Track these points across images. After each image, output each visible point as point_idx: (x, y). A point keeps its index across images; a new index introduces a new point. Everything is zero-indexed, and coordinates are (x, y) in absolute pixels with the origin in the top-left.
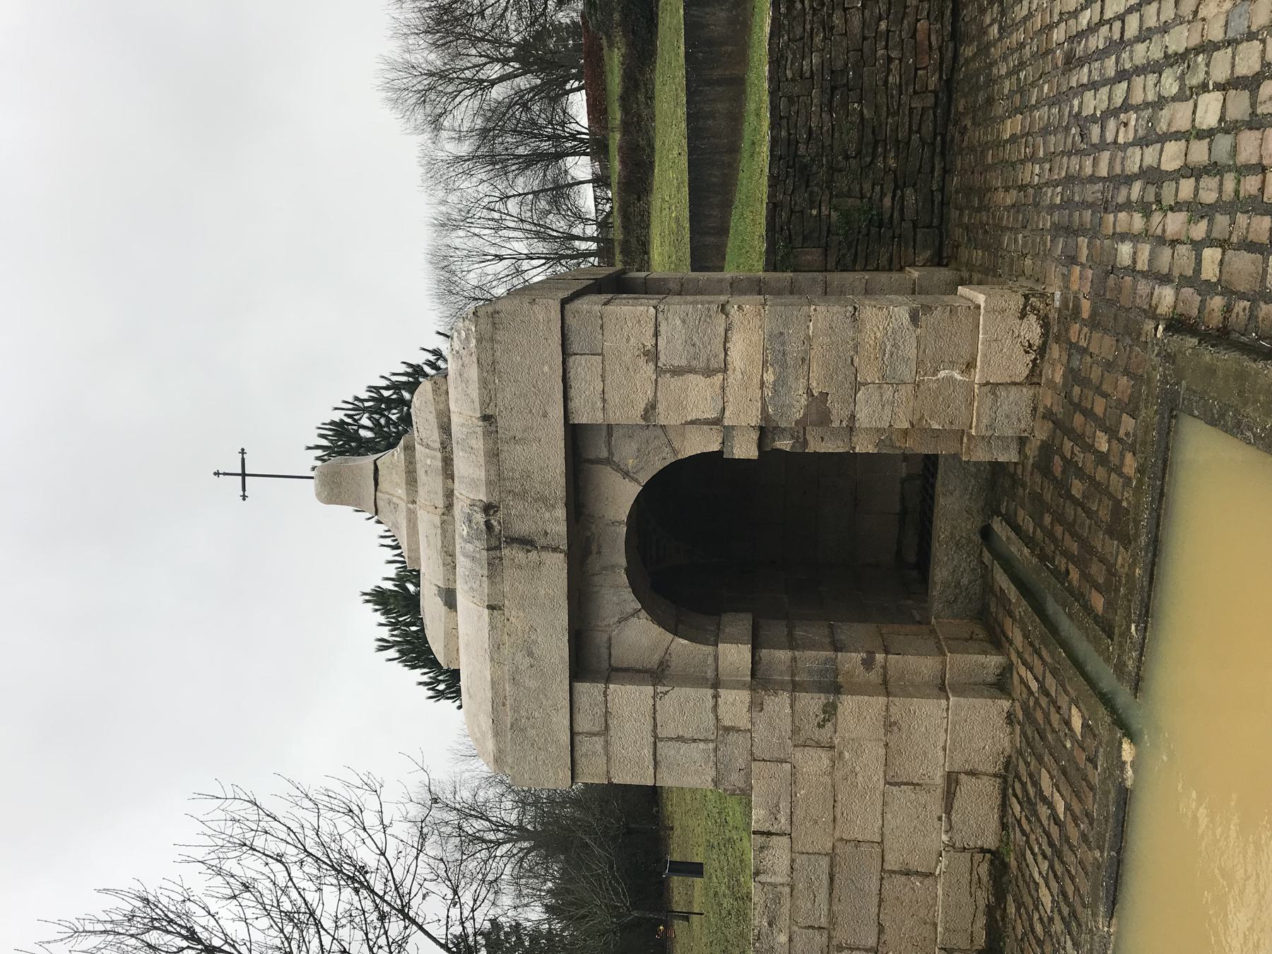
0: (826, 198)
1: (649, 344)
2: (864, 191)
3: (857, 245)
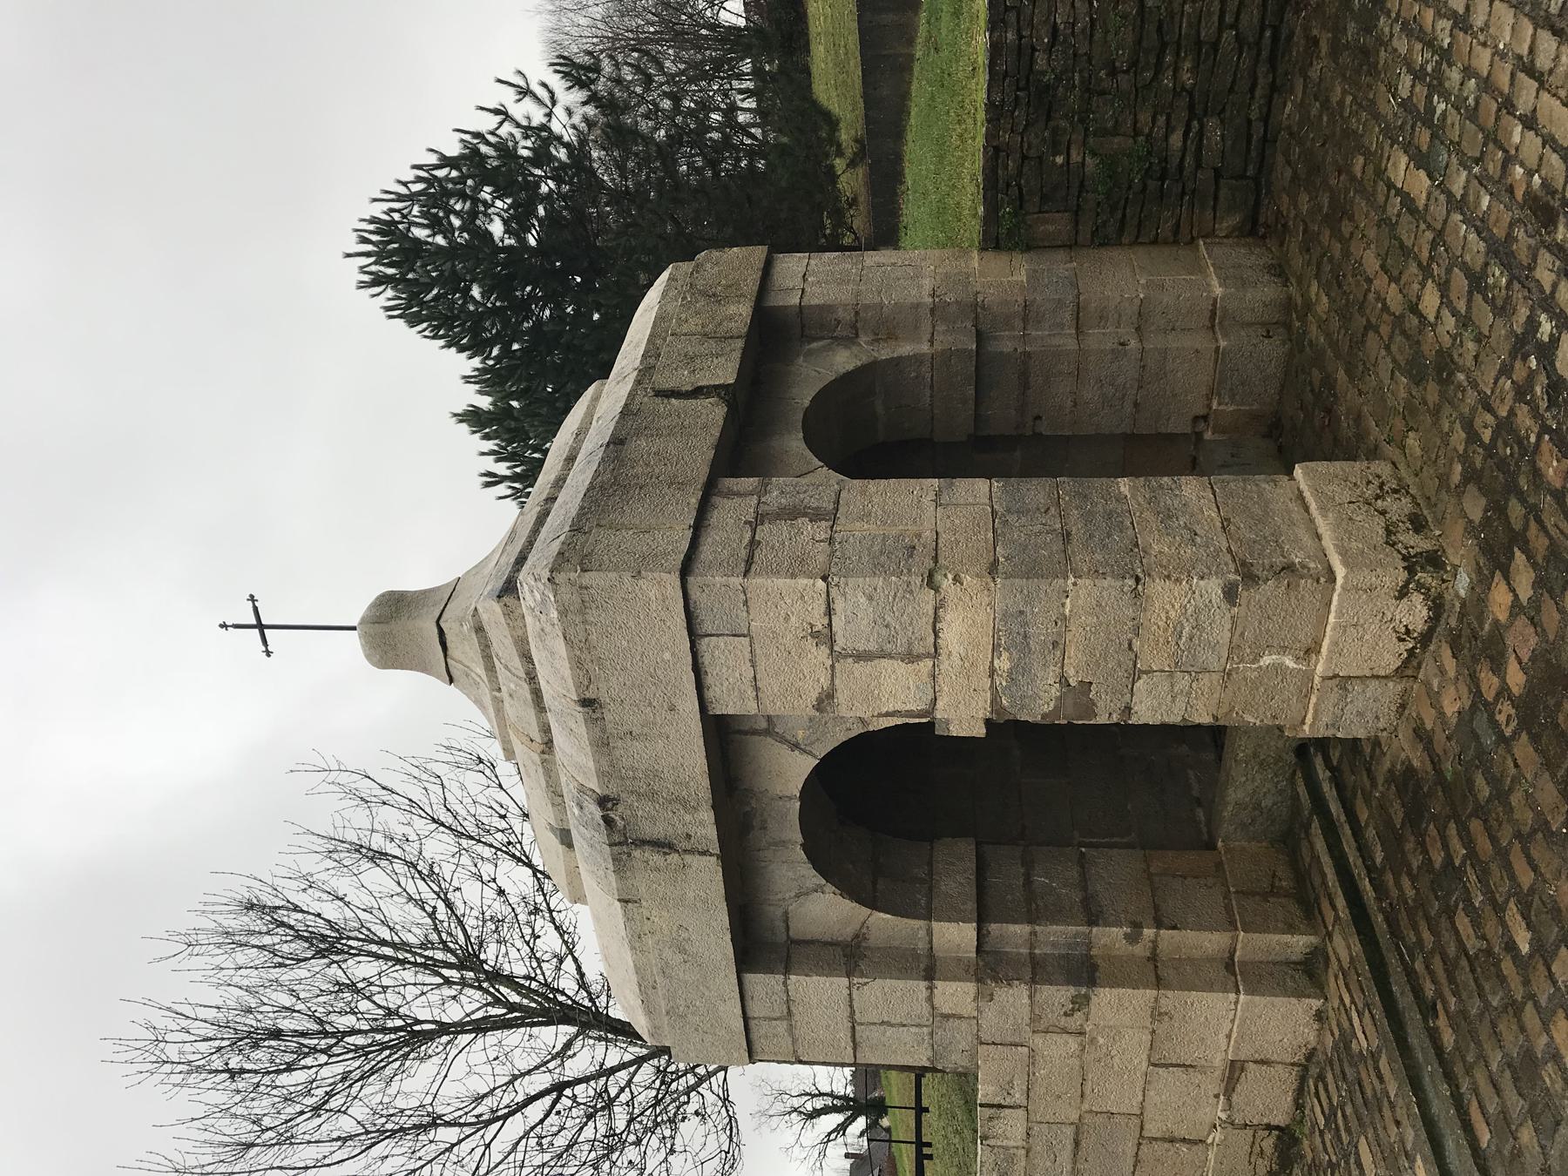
0: (1078, 137)
1: (820, 624)
2: (1138, 125)
3: (1125, 208)
